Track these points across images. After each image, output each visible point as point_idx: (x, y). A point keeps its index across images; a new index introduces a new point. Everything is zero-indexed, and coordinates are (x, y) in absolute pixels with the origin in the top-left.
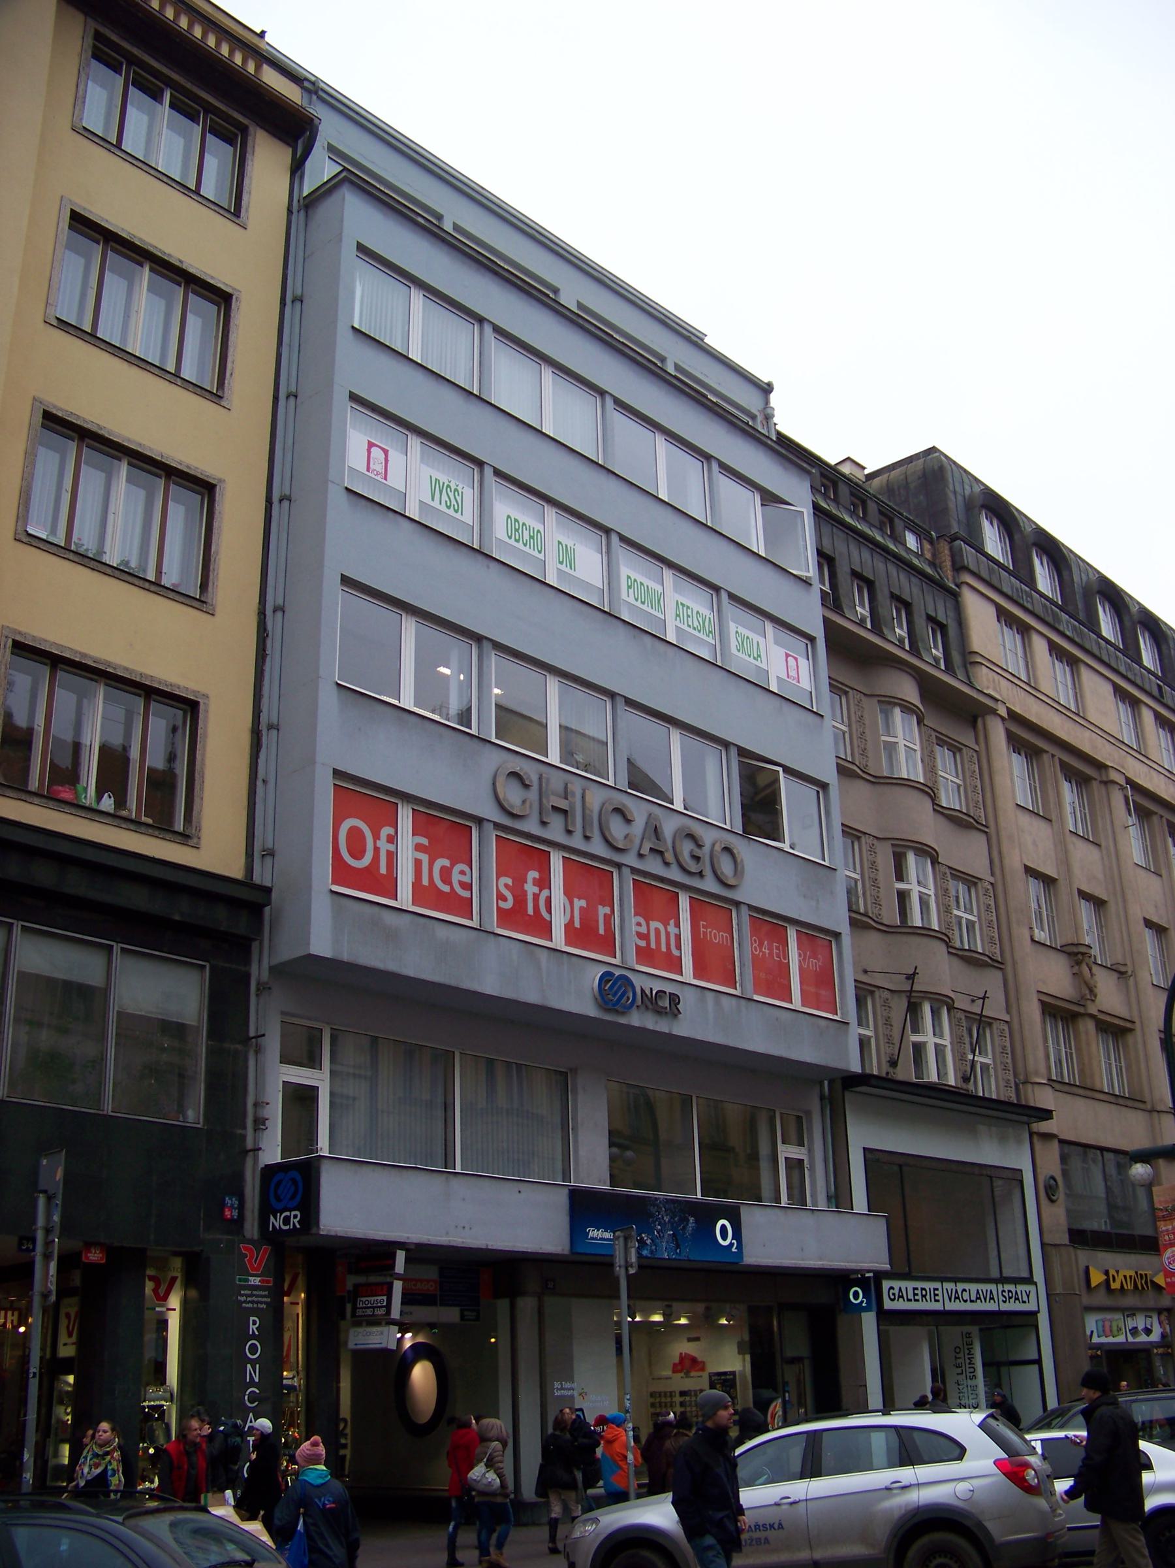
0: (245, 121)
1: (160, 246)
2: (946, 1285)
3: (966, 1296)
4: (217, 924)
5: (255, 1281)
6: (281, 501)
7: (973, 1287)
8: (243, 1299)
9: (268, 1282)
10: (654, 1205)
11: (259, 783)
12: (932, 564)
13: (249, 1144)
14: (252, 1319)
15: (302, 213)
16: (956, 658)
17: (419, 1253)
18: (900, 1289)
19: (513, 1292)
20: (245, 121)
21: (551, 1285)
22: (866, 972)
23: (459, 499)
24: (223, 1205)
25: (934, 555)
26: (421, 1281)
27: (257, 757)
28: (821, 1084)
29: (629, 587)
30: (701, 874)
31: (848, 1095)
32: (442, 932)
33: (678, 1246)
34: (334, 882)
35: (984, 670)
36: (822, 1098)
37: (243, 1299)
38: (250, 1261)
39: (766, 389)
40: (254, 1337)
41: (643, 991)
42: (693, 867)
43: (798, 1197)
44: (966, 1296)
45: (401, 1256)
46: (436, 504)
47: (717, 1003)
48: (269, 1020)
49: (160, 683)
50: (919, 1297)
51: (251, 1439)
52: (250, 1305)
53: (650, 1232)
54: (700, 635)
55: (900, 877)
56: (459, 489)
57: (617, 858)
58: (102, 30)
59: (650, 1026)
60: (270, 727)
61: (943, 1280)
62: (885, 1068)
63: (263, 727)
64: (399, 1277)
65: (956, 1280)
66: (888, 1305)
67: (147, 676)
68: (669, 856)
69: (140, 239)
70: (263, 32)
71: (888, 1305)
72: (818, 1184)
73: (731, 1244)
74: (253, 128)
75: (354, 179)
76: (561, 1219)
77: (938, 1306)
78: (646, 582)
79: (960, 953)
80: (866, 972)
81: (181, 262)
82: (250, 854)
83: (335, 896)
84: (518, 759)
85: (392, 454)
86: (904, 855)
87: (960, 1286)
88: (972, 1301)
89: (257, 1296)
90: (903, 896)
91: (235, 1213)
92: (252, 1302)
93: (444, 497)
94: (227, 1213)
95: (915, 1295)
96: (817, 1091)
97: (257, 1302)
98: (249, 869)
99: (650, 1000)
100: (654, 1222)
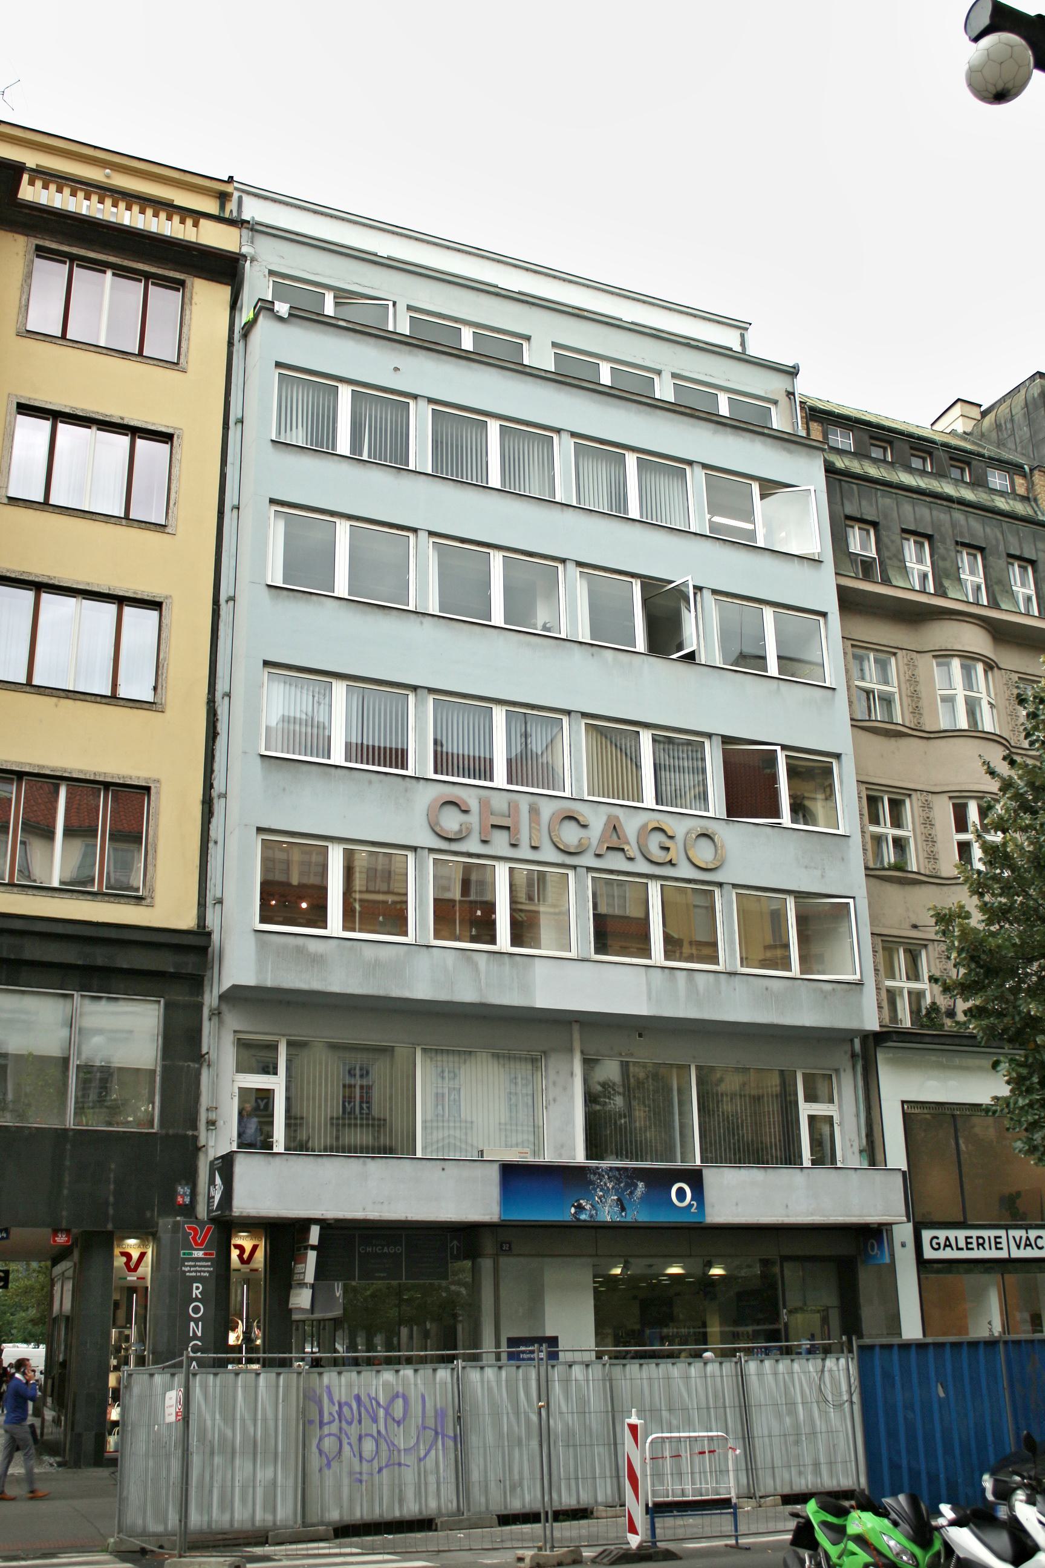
1: (101, 411)
2: (1012, 1233)
4: (171, 966)
5: (200, 1254)
6: (227, 602)
9: (211, 1254)
10: (595, 1174)
11: (211, 845)
12: (1025, 499)
14: (195, 1285)
15: (242, 343)
18: (947, 1239)
19: (472, 1253)
22: (915, 927)
24: (174, 1193)
25: (1028, 490)
27: (209, 822)
28: (852, 1041)
30: (671, 863)
31: (879, 1050)
32: (369, 952)
33: (623, 1209)
34: (263, 920)
36: (853, 1056)
39: (792, 372)
40: (196, 1321)
42: (658, 855)
43: (824, 1155)
47: (690, 981)
48: (220, 1043)
50: (975, 1245)
52: (194, 1274)
57: (569, 860)
58: (41, 242)
60: (219, 796)
64: (313, 1248)
66: (929, 1254)
68: (633, 850)
69: (82, 410)
70: (231, 178)
71: (929, 1254)
72: (847, 1142)
73: (690, 1205)
74: (189, 280)
76: (493, 1190)
80: (915, 927)
81: (122, 418)
82: (202, 905)
84: (456, 788)
86: (965, 806)
91: (187, 1200)
92: (196, 1271)
94: (180, 1200)
95: (967, 1243)
96: (848, 1048)
97: (200, 1272)
100: (595, 1190)
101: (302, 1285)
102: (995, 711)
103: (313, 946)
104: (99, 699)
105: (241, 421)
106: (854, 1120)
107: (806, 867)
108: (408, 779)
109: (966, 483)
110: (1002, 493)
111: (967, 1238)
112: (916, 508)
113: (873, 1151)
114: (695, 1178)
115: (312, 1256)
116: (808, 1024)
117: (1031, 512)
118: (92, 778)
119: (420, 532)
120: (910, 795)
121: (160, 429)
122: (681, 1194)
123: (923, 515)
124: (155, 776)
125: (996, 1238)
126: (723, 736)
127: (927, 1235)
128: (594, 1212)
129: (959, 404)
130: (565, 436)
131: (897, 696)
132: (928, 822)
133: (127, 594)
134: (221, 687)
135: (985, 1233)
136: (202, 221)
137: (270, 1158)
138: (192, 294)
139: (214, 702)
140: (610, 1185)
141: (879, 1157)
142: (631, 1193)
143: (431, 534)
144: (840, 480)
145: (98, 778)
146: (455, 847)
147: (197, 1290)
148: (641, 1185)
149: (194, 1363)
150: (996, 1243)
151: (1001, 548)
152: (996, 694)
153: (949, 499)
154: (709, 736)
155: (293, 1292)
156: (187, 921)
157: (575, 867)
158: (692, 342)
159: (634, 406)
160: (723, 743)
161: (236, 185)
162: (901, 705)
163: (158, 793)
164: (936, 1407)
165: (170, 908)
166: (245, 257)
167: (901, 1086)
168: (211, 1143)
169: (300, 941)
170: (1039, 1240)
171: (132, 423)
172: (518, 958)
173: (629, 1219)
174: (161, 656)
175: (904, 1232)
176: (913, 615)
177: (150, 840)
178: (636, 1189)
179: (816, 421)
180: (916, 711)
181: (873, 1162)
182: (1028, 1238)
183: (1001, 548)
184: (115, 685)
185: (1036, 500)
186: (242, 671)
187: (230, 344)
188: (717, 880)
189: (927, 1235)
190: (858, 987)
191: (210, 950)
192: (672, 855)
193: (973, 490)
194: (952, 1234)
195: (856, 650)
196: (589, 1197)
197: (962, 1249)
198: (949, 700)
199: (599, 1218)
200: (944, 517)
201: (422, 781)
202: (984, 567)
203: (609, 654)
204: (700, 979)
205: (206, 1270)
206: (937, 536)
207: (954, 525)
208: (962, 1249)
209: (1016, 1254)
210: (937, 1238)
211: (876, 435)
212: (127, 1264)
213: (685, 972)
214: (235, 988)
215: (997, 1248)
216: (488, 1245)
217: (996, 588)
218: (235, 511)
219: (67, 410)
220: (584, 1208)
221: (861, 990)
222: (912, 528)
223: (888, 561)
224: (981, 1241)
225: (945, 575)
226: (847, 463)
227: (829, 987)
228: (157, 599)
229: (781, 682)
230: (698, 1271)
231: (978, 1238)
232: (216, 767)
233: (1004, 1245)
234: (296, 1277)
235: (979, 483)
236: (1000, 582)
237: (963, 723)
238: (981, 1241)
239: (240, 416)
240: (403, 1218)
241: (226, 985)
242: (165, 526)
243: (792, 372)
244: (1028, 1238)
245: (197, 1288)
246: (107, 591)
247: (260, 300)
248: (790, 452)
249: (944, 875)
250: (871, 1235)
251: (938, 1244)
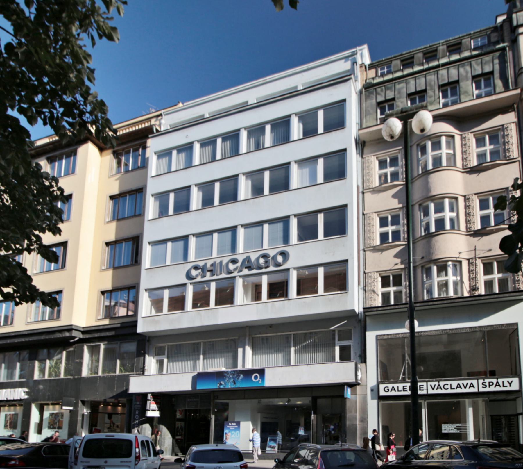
3: (446, 387)
18: (393, 387)
33: (235, 383)
44: (446, 387)
64: (414, 388)
73: (259, 381)
95: (404, 389)
114: (261, 372)
140: (231, 376)
142: (238, 378)
147: (137, 413)
164: (80, 418)
173: (237, 387)
196: (224, 380)
199: (227, 387)
209: (431, 392)
251: (388, 390)
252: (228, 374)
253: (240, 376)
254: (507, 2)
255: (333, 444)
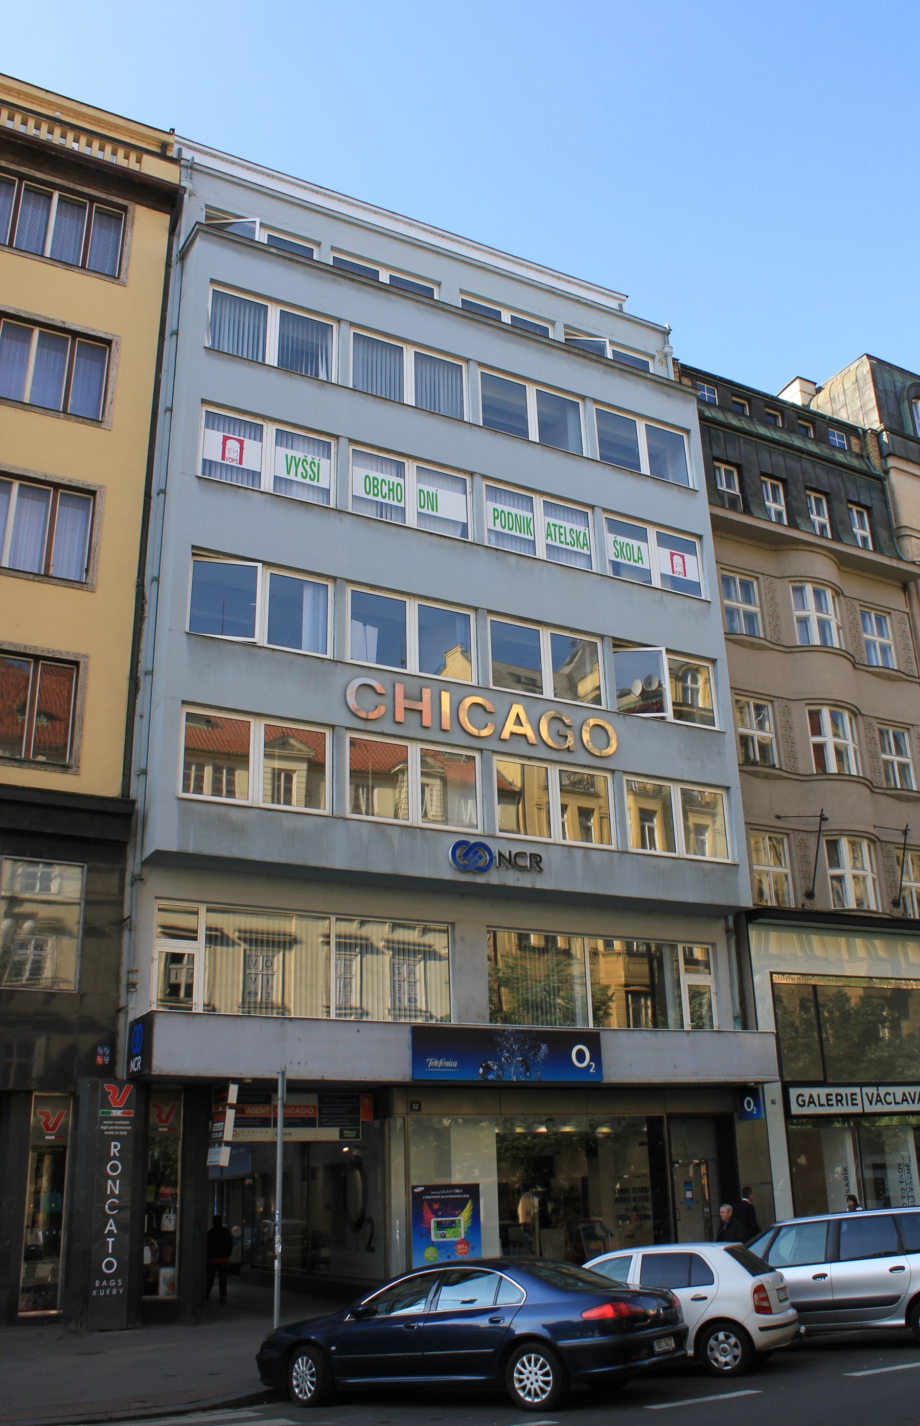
0: (125, 203)
2: (865, 1090)
3: (890, 1099)
4: (98, 832)
5: (119, 1113)
6: (158, 494)
7: (899, 1091)
8: (105, 1128)
9: (129, 1113)
10: (501, 1037)
11: (137, 718)
12: (859, 456)
13: (122, 1003)
14: (113, 1144)
16: (883, 533)
17: (296, 1087)
18: (811, 1096)
20: (125, 203)
21: (416, 1107)
22: (778, 817)
23: (315, 469)
25: (861, 448)
26: (300, 1107)
27: (136, 698)
28: (726, 918)
29: (495, 518)
31: (750, 926)
33: (528, 1070)
35: (914, 540)
36: (727, 931)
37: (105, 1128)
38: (113, 1098)
39: (666, 333)
40: (115, 1158)
41: (500, 854)
44: (890, 1099)
45: (233, 1090)
46: (292, 477)
49: (43, 651)
50: (834, 1102)
51: (110, 1240)
52: (112, 1133)
53: (497, 1059)
54: (575, 549)
55: (817, 730)
56: (316, 461)
59: (511, 883)
60: (146, 673)
61: (861, 1085)
62: (802, 899)
63: (141, 673)
64: (232, 1106)
65: (877, 1085)
66: (795, 1110)
67: (30, 647)
69: (25, 312)
71: (795, 1110)
72: (722, 1010)
73: (589, 1066)
74: (131, 206)
75: (218, 227)
77: (858, 1110)
78: (514, 511)
79: (888, 792)
80: (778, 817)
82: (127, 775)
83: (181, 801)
85: (247, 442)
87: (883, 1090)
88: (896, 1103)
89: (118, 1125)
90: (819, 749)
91: (107, 1060)
92: (114, 1130)
93: (300, 469)
95: (828, 1100)
97: (119, 1130)
98: (126, 786)
99: (510, 861)
100: (502, 1051)
101: (220, 1142)
102: (841, 631)
103: (234, 814)
104: (31, 577)
105: (176, 333)
106: (728, 989)
107: (688, 759)
108: (326, 662)
109: (810, 438)
110: (841, 450)
111: (827, 1095)
112: (773, 457)
113: (745, 1018)
114: (593, 1040)
115: (230, 1114)
116: (691, 900)
117: (865, 468)
118: (22, 650)
119: (341, 440)
120: (889, 614)
121: (99, 335)
122: (581, 1056)
123: (778, 462)
124: (83, 652)
125: (852, 1095)
126: (614, 638)
127: (794, 1092)
128: (500, 1072)
129: (798, 381)
130: (473, 365)
131: (759, 616)
132: (788, 725)
133: (62, 482)
134: (149, 573)
135: (843, 1091)
136: (145, 157)
137: (190, 1018)
138: (133, 218)
139: (143, 586)
140: (515, 1047)
141: (751, 1021)
142: (536, 1054)
143: (352, 441)
144: (709, 427)
145: (28, 651)
146: (370, 727)
147: (115, 1149)
148: (544, 1047)
149: (111, 1220)
150: (852, 1099)
151: (843, 494)
152: (842, 618)
153: (800, 450)
154: (602, 637)
155: (210, 1150)
156: (112, 790)
157: (481, 750)
158: (582, 300)
159: (534, 344)
160: (615, 646)
161: (176, 138)
162: (763, 622)
163: (86, 668)
165: (95, 774)
166: (185, 188)
167: (779, 957)
168: (131, 1005)
169: (223, 809)
170: (888, 1096)
171: (73, 328)
172: (428, 832)
174: (93, 541)
175: (773, 1092)
176: (775, 544)
177: (77, 712)
178: (539, 1050)
179: (686, 377)
180: (776, 627)
181: (745, 1026)
182: (878, 1095)
183: (843, 494)
184: (48, 566)
185: (868, 458)
186: (187, 413)
187: (168, 265)
188: (609, 767)
189: (794, 1092)
190: (734, 868)
191: (134, 817)
192: (570, 742)
193: (817, 445)
194: (815, 1091)
195: (725, 573)
197: (824, 1105)
198: (804, 621)
200: (795, 465)
201: (340, 665)
202: (829, 510)
203: (512, 559)
204: (595, 856)
205: (125, 1128)
206: (790, 481)
207: (804, 472)
208: (824, 1105)
209: (869, 1109)
210: (803, 1096)
211: (735, 394)
212: (46, 1124)
213: (582, 851)
214: (157, 853)
215: (853, 1104)
216: (399, 1107)
217: (840, 528)
218: (168, 413)
219: (11, 311)
220: (491, 1069)
221: (737, 871)
222: (769, 471)
223: (749, 498)
224: (839, 1098)
225: (796, 515)
226: (714, 414)
227: (709, 866)
228: (92, 488)
229: (664, 593)
230: (585, 1128)
231: (837, 1095)
232: (143, 645)
233: (859, 1101)
234: (215, 1136)
235: (821, 439)
236: (842, 523)
237: (816, 640)
238: (839, 1098)
239: (175, 328)
240: (319, 1078)
241: (149, 850)
242: (101, 422)
243: (666, 333)
244: (878, 1095)
245: (116, 1147)
246: (43, 478)
247: (197, 223)
248: (668, 395)
249: (802, 772)
250: (746, 1091)
251: (803, 1101)
252: (507, 1039)
253: (539, 1048)
254: (893, 386)
255: (44, 967)
